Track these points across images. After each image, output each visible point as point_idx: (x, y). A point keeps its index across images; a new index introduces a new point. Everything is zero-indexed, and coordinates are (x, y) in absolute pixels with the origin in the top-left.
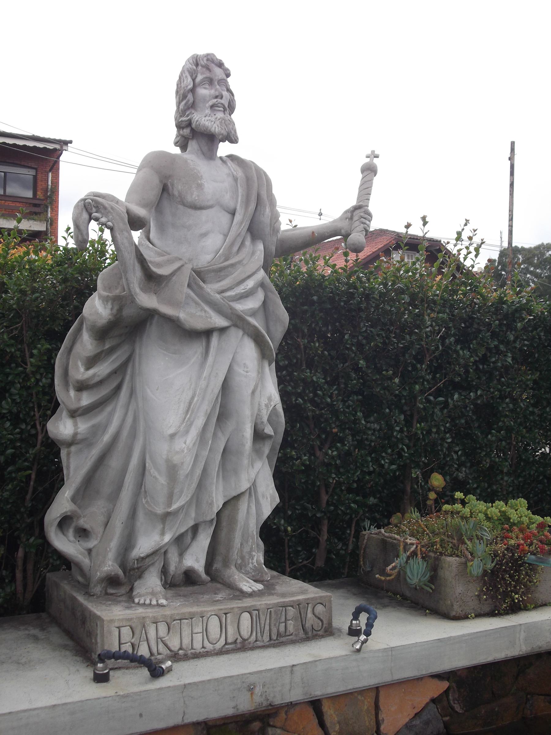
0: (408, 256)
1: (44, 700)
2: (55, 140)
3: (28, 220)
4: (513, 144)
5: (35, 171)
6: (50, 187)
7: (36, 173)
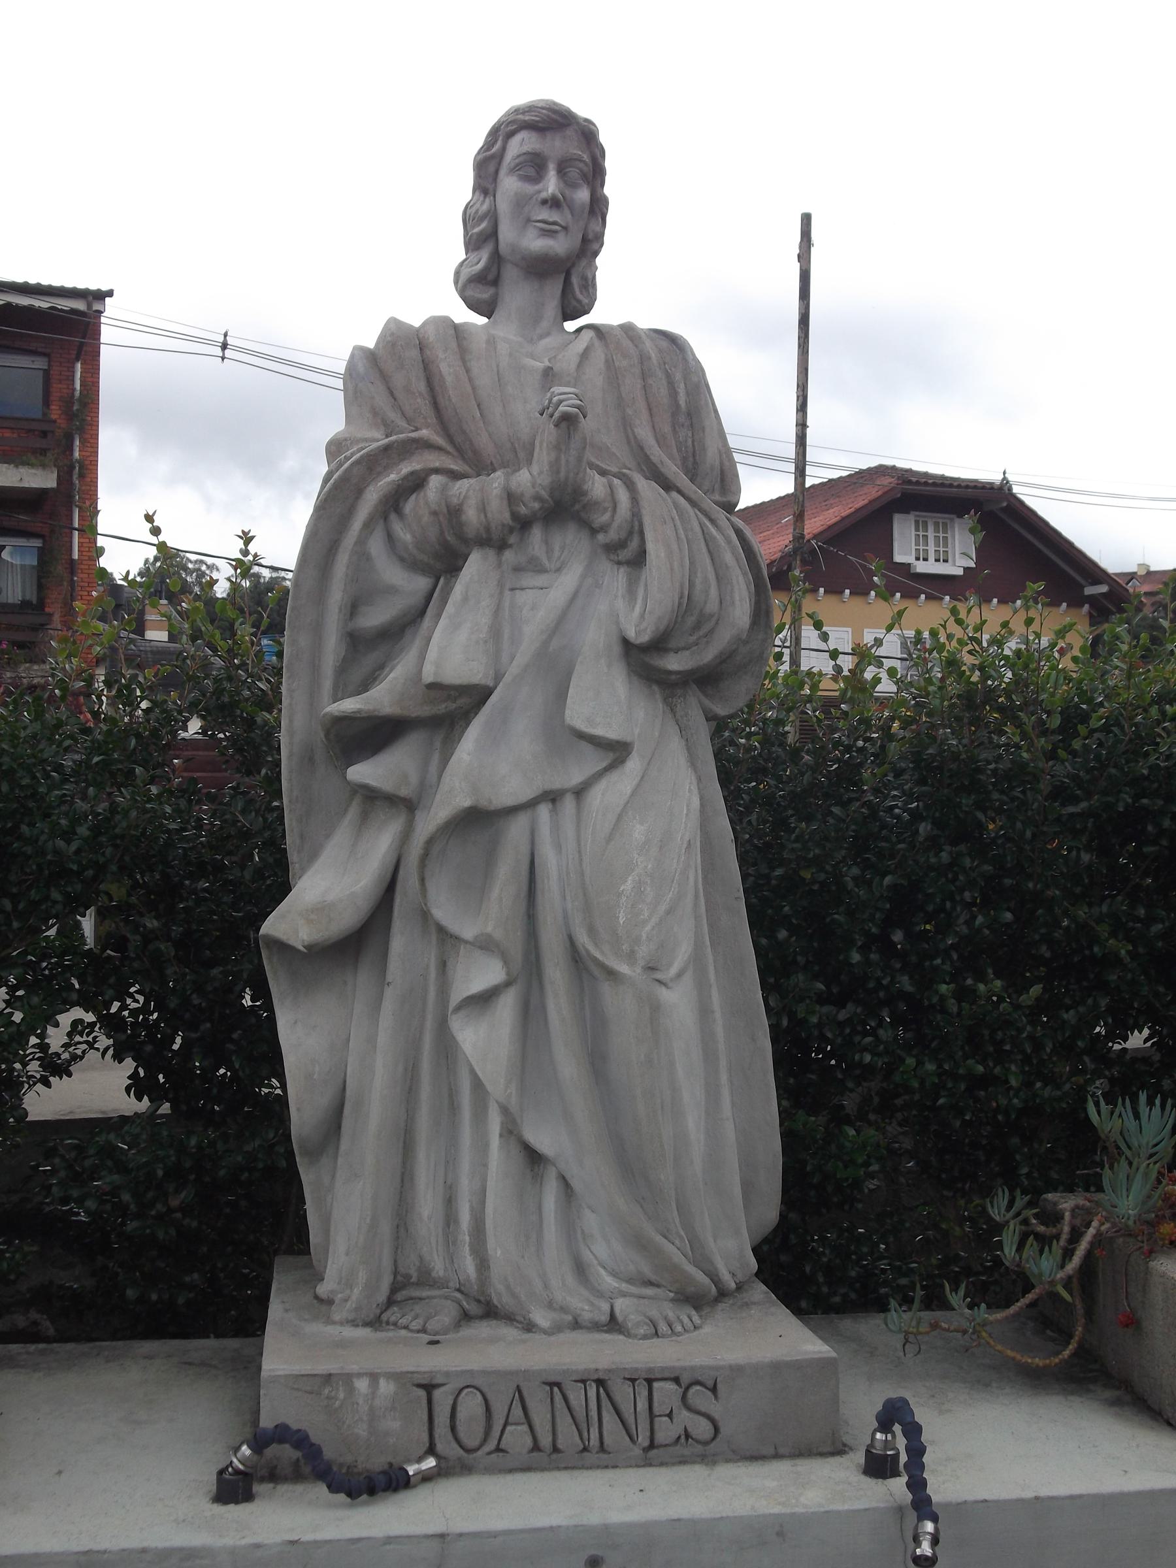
0: (936, 525)
3: (17, 466)
4: (806, 219)
5: (46, 359)
6: (77, 394)
7: (49, 365)
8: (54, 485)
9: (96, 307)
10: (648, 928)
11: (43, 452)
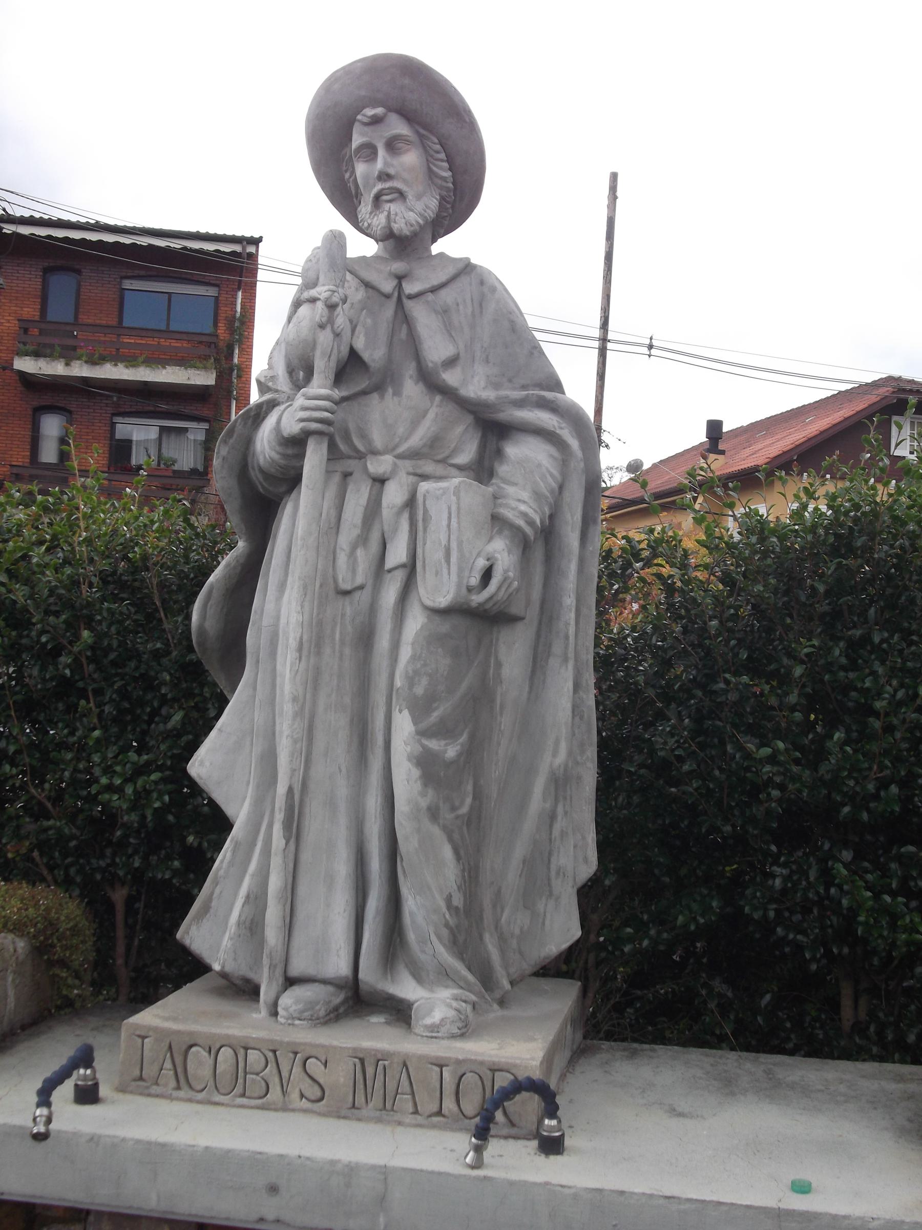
1: (377, 859)
2: (134, 228)
3: (186, 368)
4: (614, 177)
5: (217, 289)
6: (238, 315)
8: (213, 383)
9: (251, 249)
10: (162, 614)
11: (206, 358)
